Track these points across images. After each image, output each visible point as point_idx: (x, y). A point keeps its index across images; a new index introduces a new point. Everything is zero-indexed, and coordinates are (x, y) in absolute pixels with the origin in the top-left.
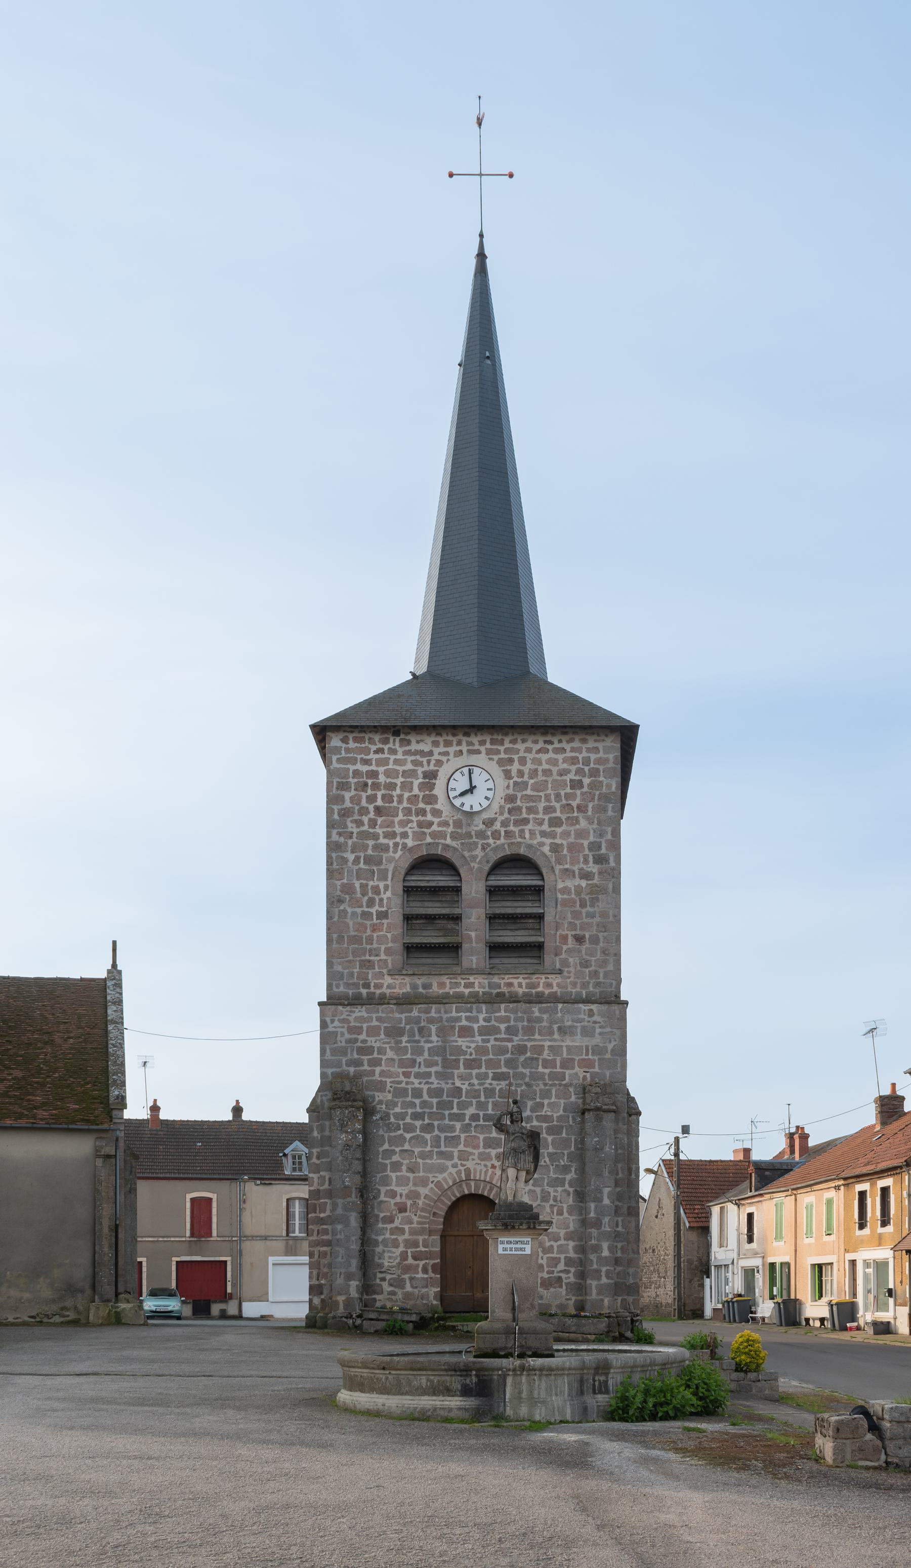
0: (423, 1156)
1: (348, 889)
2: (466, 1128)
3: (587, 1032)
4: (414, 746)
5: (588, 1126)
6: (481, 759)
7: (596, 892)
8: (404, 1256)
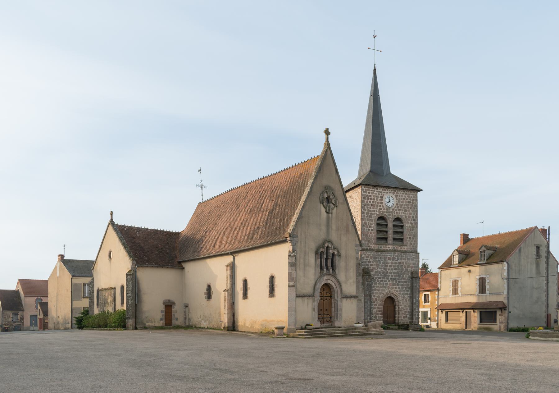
0: (381, 287)
1: (365, 223)
2: (389, 281)
3: (412, 260)
4: (379, 190)
5: (414, 281)
6: (391, 194)
7: (413, 227)
8: (377, 311)
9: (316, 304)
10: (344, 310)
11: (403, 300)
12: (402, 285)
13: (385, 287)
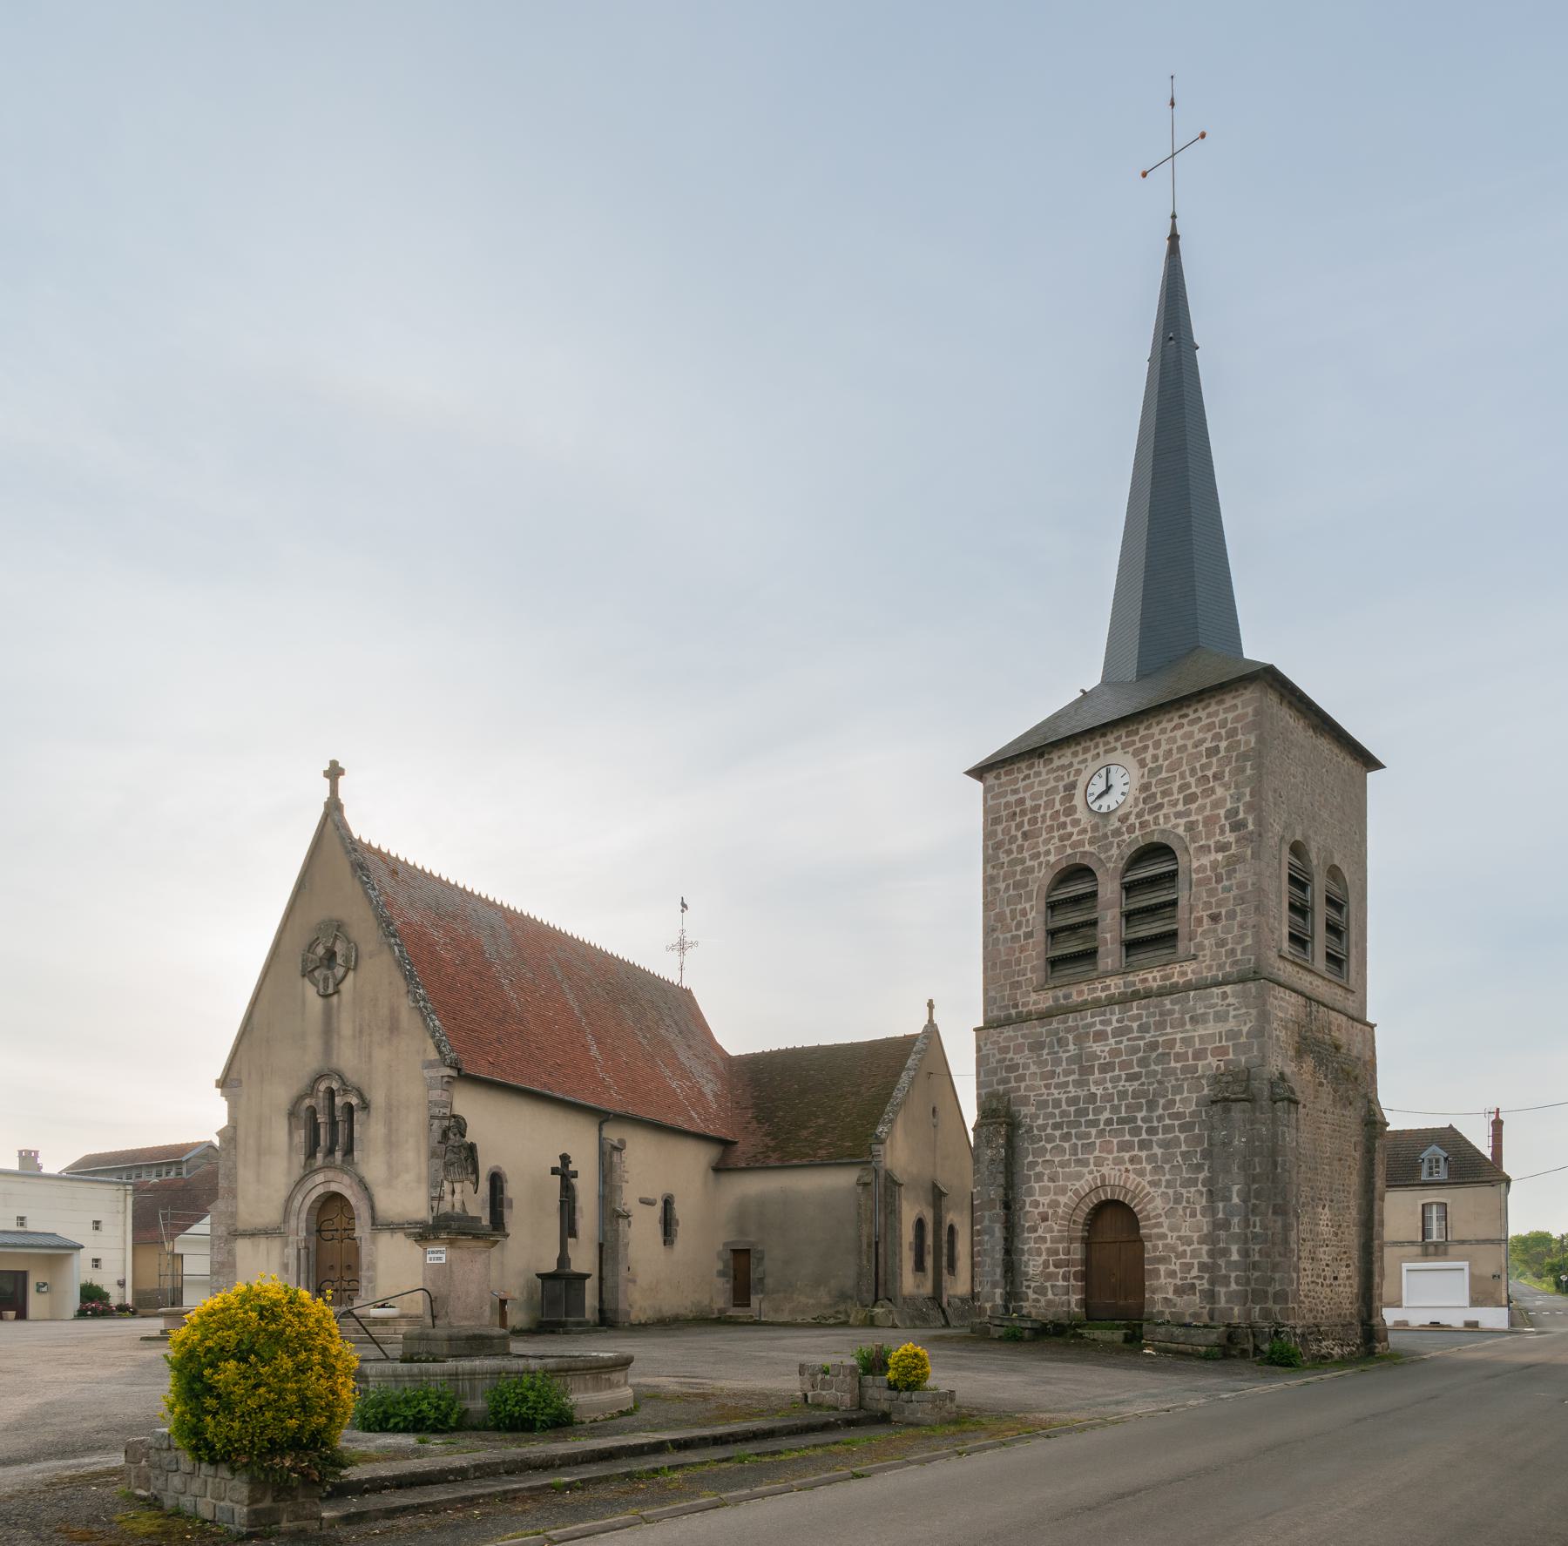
0: (1063, 1165)
2: (1101, 1133)
3: (1221, 1017)
8: (1046, 1264)
9: (291, 1252)
10: (381, 1266)
11: (1170, 1213)
12: (1165, 1145)
13: (1083, 1163)
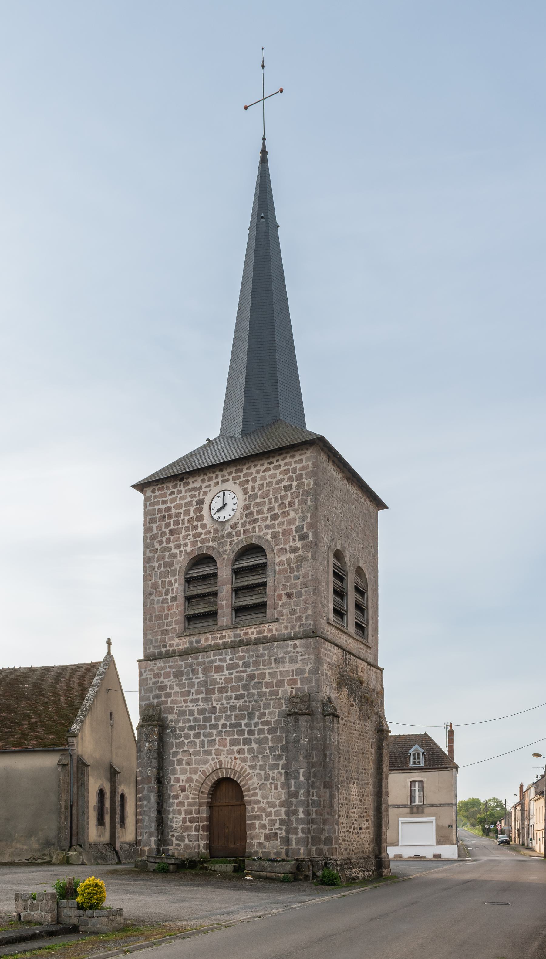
0: (195, 754)
2: (219, 734)
3: (293, 660)
4: (191, 486)
12: (259, 742)
